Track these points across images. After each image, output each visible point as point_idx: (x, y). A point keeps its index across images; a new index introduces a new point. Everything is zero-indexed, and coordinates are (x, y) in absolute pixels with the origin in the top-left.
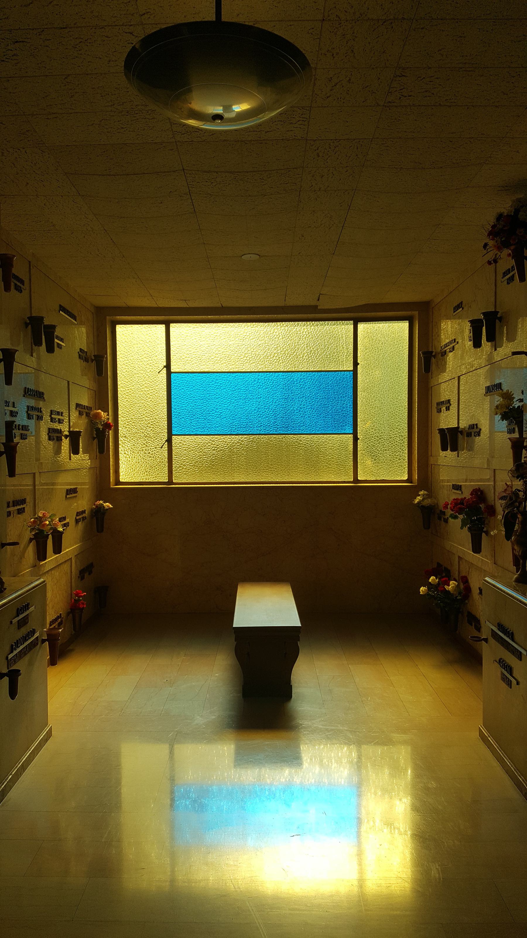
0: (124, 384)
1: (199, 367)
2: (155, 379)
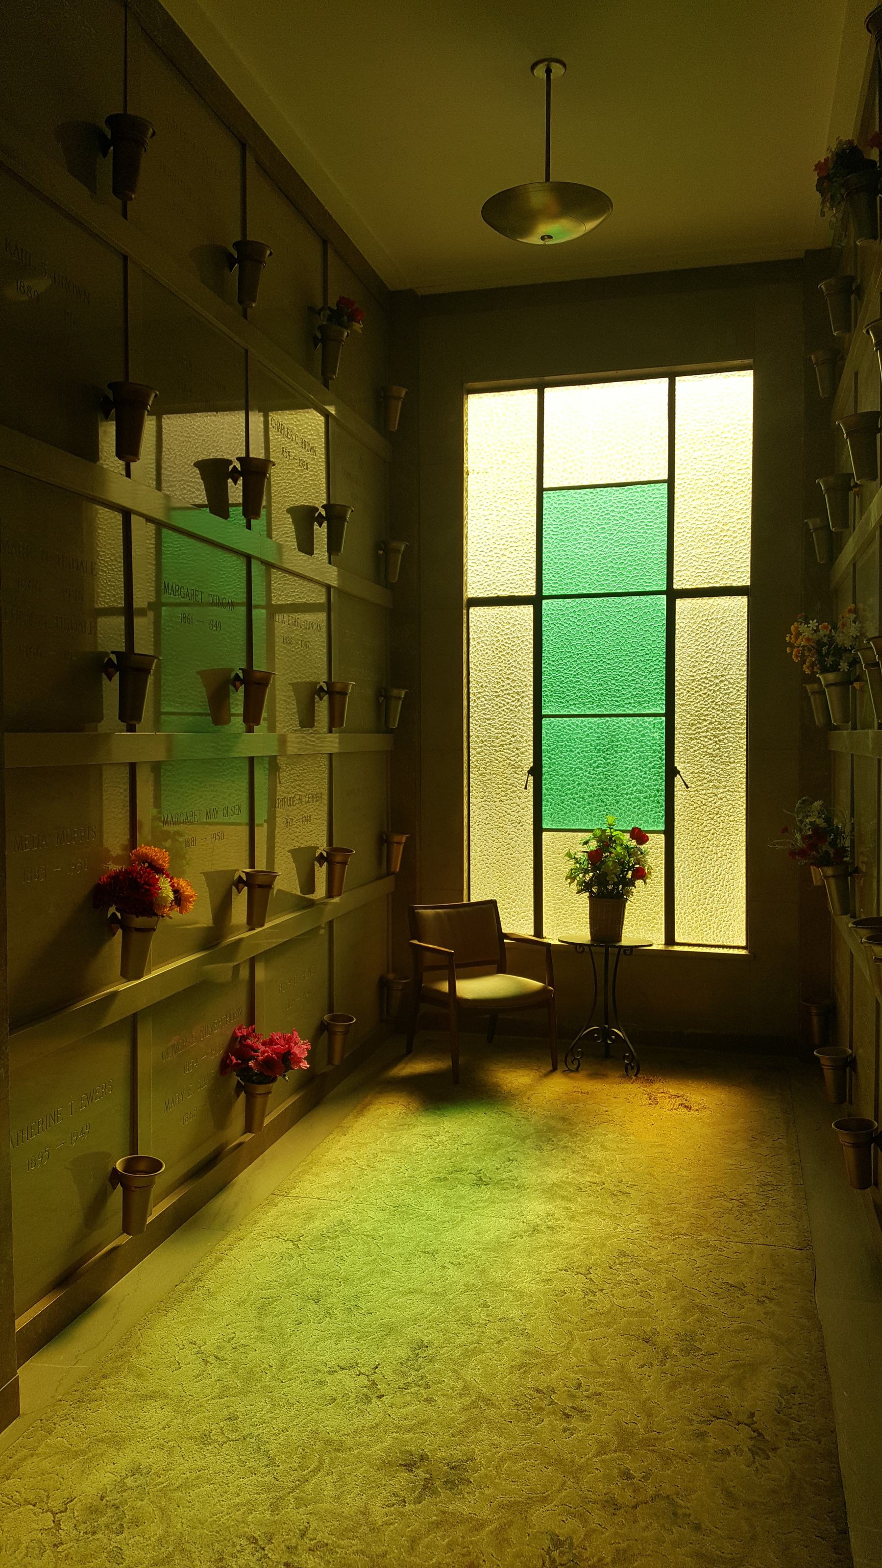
1: (688, 553)
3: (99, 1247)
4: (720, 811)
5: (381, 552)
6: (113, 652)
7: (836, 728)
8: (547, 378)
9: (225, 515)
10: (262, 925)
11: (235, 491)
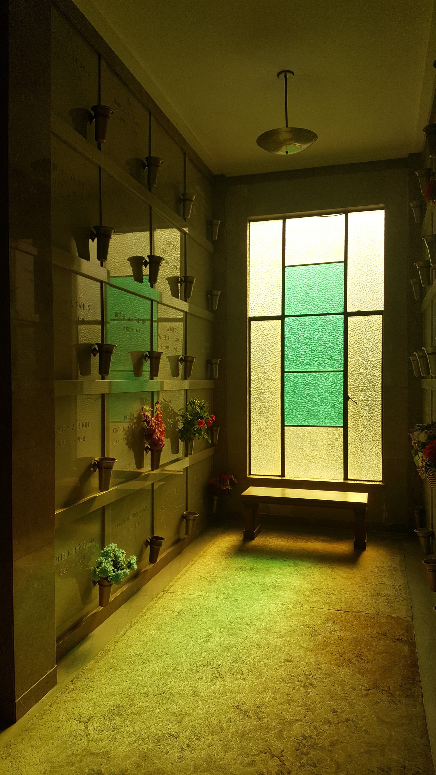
0: (273, 333)
2: (258, 330)
3: (88, 613)
4: (371, 350)
5: (209, 296)
6: (147, 352)
7: (424, 378)
8: (287, 214)
9: (141, 282)
10: (108, 490)
11: (146, 271)
